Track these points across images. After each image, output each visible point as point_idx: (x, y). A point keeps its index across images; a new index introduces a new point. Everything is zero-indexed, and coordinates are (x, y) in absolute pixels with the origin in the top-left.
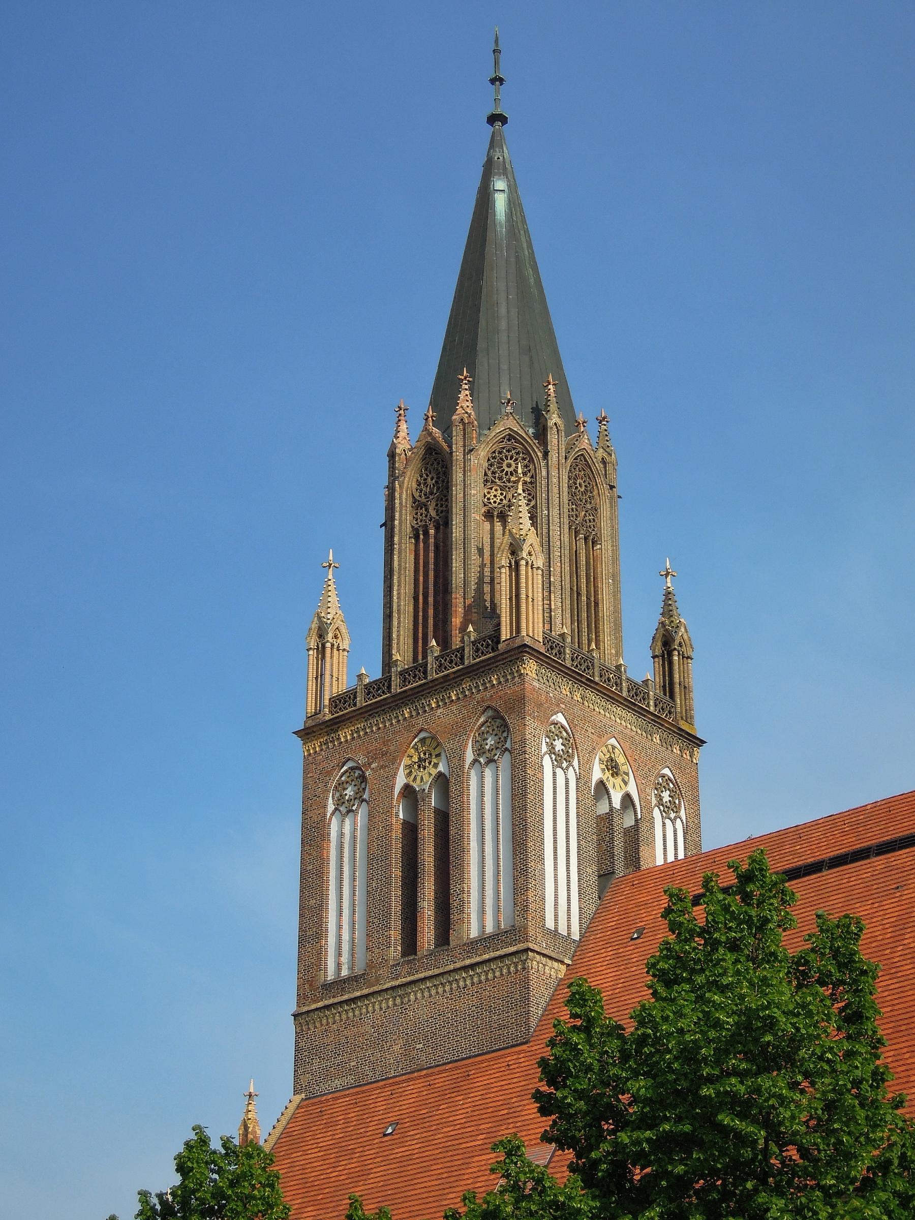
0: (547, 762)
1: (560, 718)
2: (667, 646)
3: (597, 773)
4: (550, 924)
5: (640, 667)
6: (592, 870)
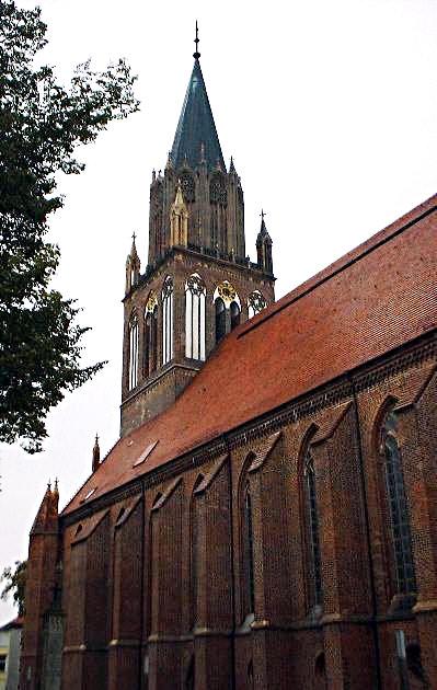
0: (188, 294)
1: (195, 275)
2: (264, 243)
3: (216, 295)
4: (188, 355)
5: (252, 253)
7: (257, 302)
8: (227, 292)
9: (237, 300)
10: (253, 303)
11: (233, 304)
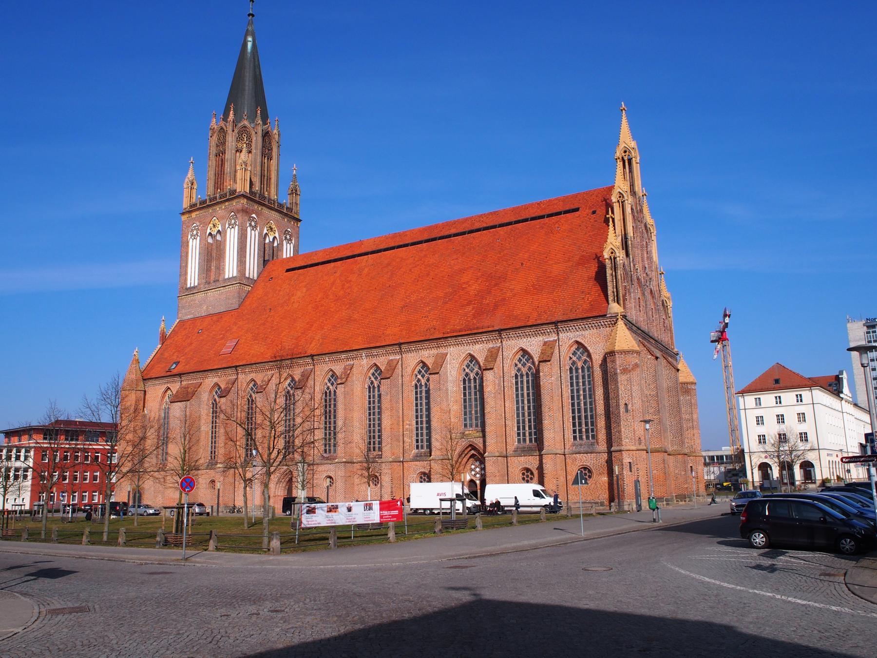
3: (265, 231)
9: (277, 235)
10: (286, 238)
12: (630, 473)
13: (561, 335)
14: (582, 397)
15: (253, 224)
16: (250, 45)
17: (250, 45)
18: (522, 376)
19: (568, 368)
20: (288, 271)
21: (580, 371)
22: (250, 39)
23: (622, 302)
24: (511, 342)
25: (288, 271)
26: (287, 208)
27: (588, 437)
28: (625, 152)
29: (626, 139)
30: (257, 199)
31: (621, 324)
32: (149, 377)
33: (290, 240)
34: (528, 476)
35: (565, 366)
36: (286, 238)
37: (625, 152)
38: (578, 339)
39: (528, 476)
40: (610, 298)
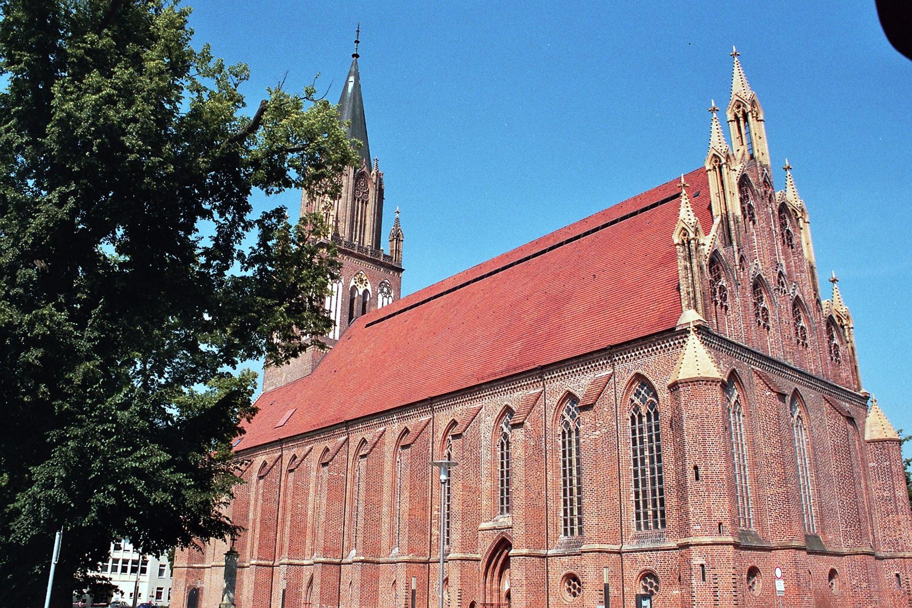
3: (352, 283)
6: (347, 316)
7: (385, 290)
8: (361, 281)
9: (369, 287)
10: (382, 291)
11: (366, 291)
12: (702, 583)
13: (617, 367)
14: (647, 461)
15: (385, 290)
16: (351, 85)
17: (351, 85)
18: (570, 432)
19: (628, 416)
20: (368, 326)
21: (645, 419)
22: (352, 79)
23: (700, 306)
24: (556, 384)
25: (368, 326)
26: (385, 256)
27: (656, 526)
28: (739, 107)
29: (740, 87)
30: (356, 252)
31: (693, 340)
32: (614, 556)
33: (389, 293)
34: (574, 587)
35: (622, 414)
36: (382, 291)
37: (739, 107)
38: (639, 371)
39: (574, 587)
40: (685, 303)
